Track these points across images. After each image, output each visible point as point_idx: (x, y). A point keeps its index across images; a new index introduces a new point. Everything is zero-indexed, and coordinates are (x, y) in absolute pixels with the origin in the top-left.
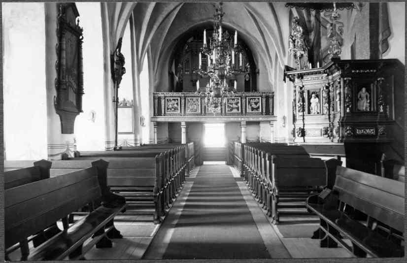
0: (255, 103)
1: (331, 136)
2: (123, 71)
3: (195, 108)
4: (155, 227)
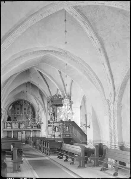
1: (61, 137)
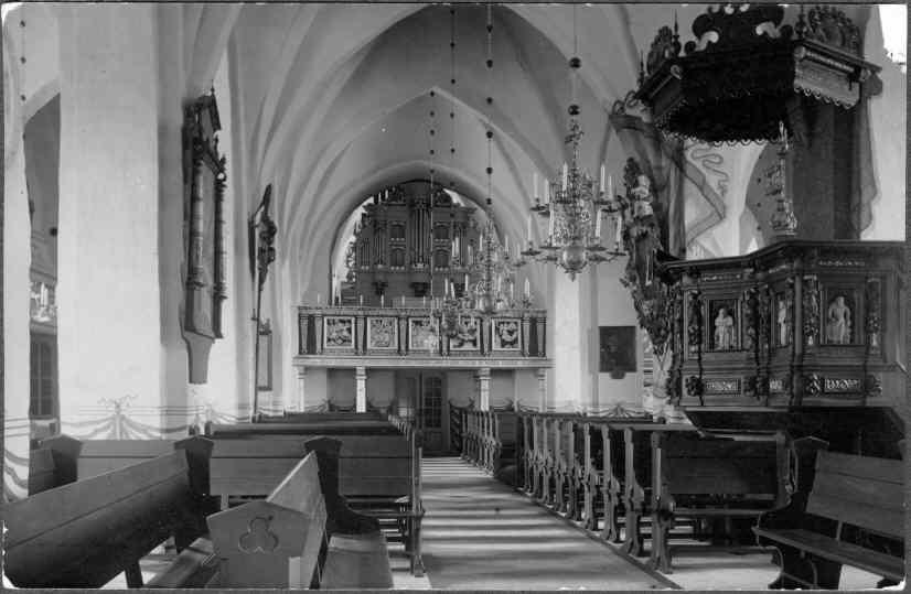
0: (509, 331)
3: (387, 340)
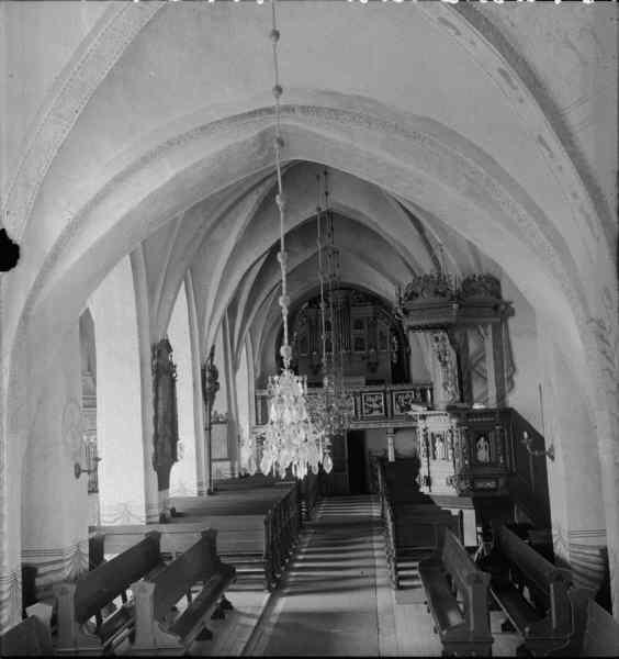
2: (216, 386)
4: (266, 596)
